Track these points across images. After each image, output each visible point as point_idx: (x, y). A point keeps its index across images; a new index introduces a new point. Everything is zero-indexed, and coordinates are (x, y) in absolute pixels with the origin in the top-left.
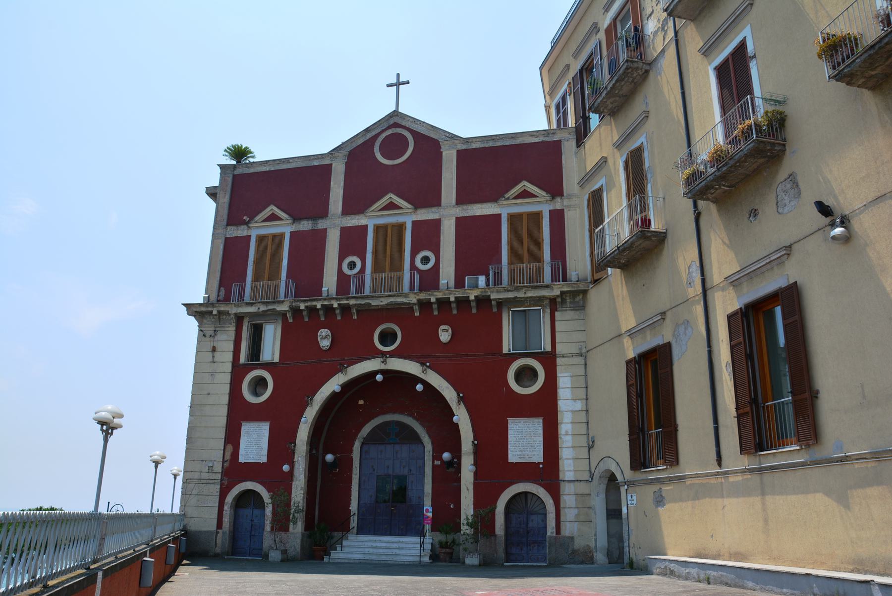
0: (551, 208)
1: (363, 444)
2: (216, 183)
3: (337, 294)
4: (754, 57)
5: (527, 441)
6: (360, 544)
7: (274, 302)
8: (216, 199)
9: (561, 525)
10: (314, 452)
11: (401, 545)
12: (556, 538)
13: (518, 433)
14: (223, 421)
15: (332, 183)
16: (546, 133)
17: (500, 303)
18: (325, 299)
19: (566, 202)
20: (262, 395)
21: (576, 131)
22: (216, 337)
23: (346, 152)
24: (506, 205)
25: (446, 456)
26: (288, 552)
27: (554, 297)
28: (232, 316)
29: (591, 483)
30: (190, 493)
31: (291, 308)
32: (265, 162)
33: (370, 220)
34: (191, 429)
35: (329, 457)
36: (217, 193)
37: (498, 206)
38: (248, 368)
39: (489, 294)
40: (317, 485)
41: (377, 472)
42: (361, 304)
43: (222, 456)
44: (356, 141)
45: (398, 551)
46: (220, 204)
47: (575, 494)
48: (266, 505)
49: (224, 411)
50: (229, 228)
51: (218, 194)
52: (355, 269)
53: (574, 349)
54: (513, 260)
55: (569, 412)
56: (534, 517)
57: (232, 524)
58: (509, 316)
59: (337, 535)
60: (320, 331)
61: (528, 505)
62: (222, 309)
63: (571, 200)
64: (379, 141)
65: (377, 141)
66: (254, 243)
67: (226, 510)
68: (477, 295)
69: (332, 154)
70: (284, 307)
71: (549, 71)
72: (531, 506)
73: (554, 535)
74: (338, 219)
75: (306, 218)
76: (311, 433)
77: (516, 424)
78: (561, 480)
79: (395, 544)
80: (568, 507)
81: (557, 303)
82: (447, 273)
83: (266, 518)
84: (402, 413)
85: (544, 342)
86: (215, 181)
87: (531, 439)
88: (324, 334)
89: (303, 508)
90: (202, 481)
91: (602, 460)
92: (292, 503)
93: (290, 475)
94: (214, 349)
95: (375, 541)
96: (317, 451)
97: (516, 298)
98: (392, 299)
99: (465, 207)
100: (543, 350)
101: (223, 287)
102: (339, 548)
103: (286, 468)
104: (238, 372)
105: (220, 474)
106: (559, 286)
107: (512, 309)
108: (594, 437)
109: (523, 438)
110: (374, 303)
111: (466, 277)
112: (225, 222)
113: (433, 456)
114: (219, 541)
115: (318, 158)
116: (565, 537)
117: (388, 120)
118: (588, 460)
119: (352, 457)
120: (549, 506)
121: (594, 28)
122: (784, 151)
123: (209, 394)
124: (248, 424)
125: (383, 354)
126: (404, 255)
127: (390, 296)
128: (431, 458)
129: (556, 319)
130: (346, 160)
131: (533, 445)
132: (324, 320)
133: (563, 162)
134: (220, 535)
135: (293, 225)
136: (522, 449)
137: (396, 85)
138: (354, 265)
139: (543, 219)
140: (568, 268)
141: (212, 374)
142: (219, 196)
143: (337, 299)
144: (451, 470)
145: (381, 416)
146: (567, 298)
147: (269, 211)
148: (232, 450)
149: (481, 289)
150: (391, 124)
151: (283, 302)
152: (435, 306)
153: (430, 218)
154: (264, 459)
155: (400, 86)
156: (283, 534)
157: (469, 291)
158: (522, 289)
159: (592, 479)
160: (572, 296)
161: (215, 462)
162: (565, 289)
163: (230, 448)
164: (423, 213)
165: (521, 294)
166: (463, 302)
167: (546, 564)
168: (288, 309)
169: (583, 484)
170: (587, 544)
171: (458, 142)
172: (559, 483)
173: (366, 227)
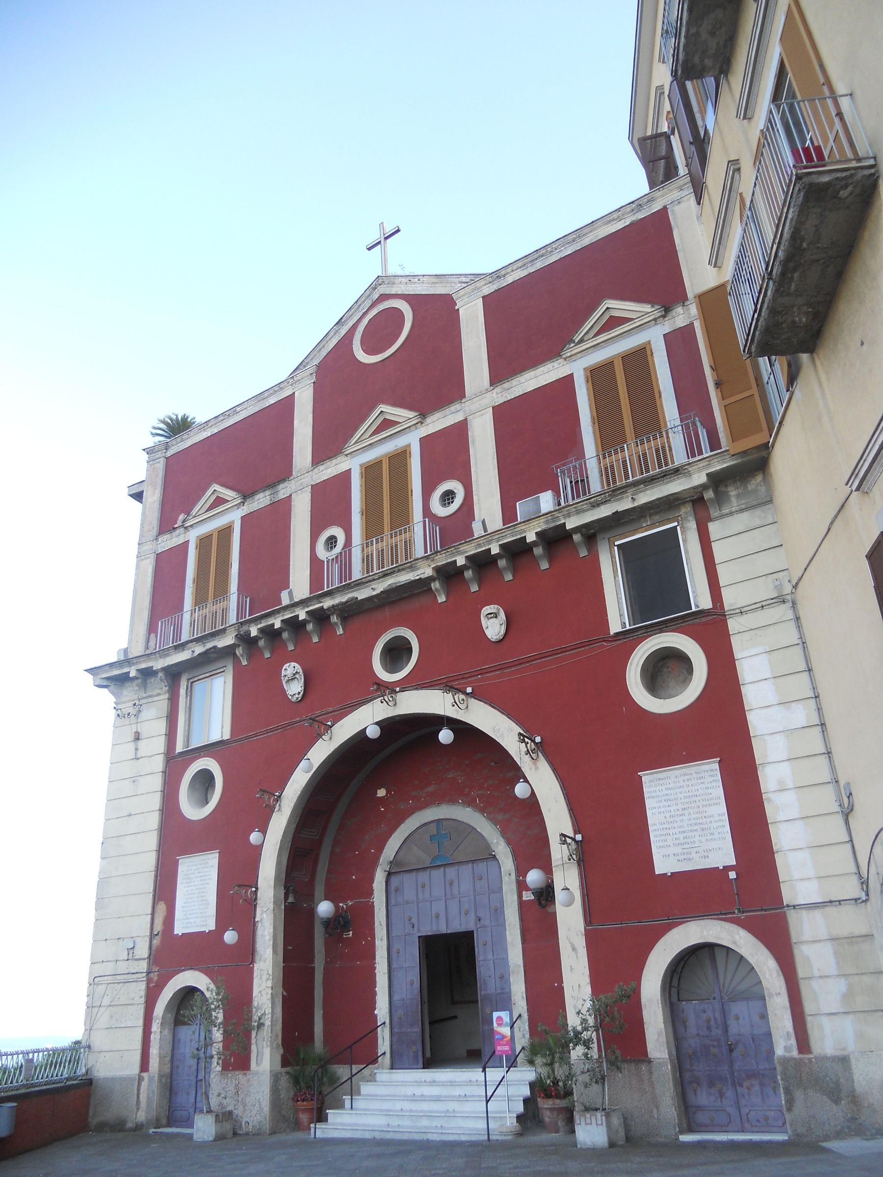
0: (667, 329)
1: (389, 874)
5: (690, 820)
9: (809, 1025)
13: (667, 804)
14: (151, 860)
16: (637, 204)
21: (692, 181)
23: (311, 368)
25: (534, 877)
29: (868, 903)
34: (103, 882)
39: (563, 522)
40: (313, 969)
41: (419, 931)
43: (149, 925)
46: (147, 506)
47: (833, 939)
53: (764, 591)
55: (778, 736)
56: (738, 1008)
59: (342, 1071)
60: (284, 668)
61: (721, 981)
67: (155, 1032)
68: (539, 530)
73: (795, 1053)
76: (285, 862)
77: (661, 782)
78: (788, 906)
84: (453, 801)
90: (118, 977)
91: (877, 837)
99: (506, 385)
100: (694, 609)
106: (701, 464)
107: (616, 543)
108: (848, 784)
109: (680, 812)
111: (517, 504)
112: (155, 532)
116: (823, 1058)
118: (849, 846)
120: (767, 976)
123: (130, 815)
126: (412, 500)
128: (514, 886)
129: (713, 537)
131: (705, 826)
133: (677, 241)
134: (144, 1084)
141: (134, 780)
145: (416, 814)
158: (626, 492)
159: (867, 895)
162: (717, 467)
163: (162, 907)
169: (848, 909)
171: (483, 282)
172: (785, 915)
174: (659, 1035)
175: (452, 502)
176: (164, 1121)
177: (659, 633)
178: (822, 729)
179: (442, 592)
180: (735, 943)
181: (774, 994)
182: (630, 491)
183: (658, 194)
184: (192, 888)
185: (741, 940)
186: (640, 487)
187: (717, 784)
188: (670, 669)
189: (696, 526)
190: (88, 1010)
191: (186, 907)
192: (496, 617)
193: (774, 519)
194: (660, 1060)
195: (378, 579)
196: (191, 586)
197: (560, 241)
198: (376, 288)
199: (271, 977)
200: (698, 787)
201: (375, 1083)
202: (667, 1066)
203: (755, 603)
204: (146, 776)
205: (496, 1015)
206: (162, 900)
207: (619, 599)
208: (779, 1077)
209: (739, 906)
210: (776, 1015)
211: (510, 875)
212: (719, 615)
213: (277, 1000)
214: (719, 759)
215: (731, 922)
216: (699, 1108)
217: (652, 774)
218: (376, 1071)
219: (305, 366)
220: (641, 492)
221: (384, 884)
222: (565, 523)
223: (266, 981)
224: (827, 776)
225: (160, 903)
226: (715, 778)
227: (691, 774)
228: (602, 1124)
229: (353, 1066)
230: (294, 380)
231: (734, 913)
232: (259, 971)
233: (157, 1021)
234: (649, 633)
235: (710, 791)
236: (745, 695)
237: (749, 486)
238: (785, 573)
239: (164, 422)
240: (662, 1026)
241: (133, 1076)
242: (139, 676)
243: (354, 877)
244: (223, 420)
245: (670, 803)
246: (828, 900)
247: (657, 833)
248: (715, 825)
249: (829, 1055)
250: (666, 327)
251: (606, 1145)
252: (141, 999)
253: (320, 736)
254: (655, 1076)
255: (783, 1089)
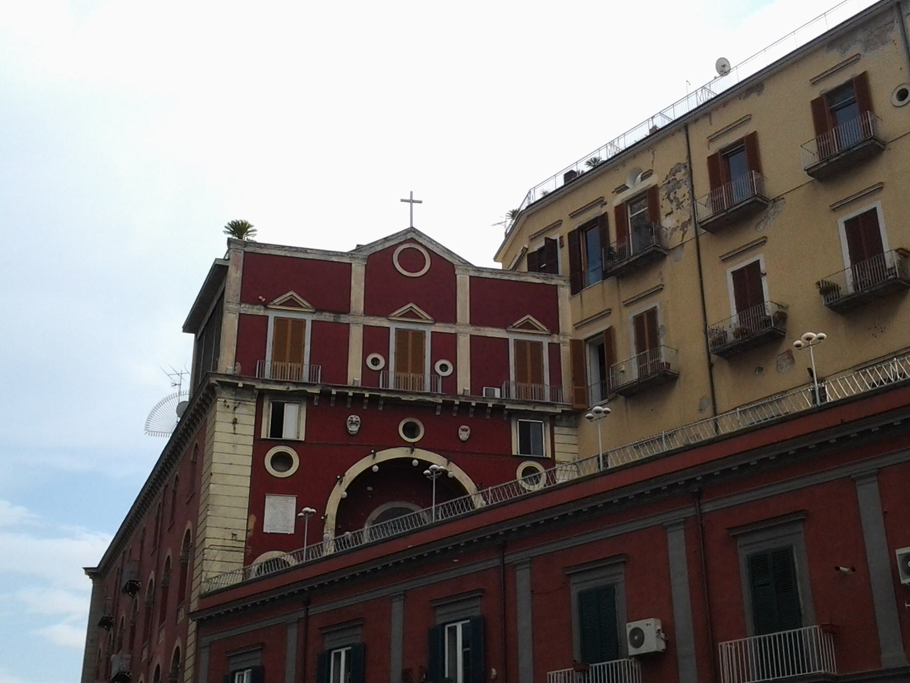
4: (765, 274)
33: (392, 325)
38: (269, 444)
60: (351, 416)
64: (397, 252)
69: (351, 254)
82: (464, 383)
84: (410, 501)
88: (354, 419)
94: (235, 422)
104: (260, 448)
107: (519, 420)
117: (405, 234)
122: (784, 336)
163: (253, 518)
166: (482, 407)
205: (720, 644)
219: (360, 252)
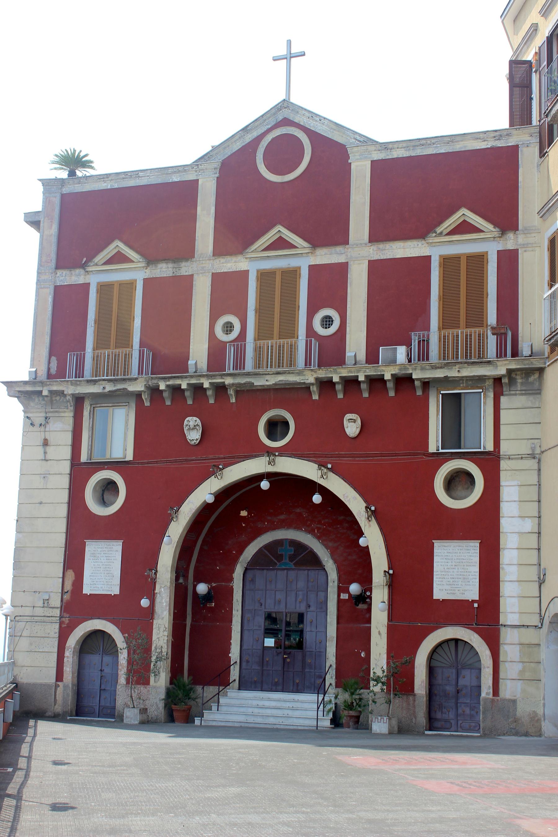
2: (38, 207)
3: (209, 369)
5: (458, 572)
6: (243, 702)
7: (124, 380)
8: (39, 230)
9: (500, 683)
10: (181, 581)
11: (295, 705)
12: (493, 700)
13: (446, 561)
14: (61, 539)
15: (199, 209)
16: (498, 134)
17: (426, 384)
18: (192, 377)
19: (521, 239)
20: (112, 503)
22: (48, 426)
23: (216, 163)
24: (438, 244)
25: (355, 588)
26: (148, 711)
27: (499, 377)
28: (68, 398)
29: (541, 629)
30: (19, 634)
31: (148, 387)
32: (105, 177)
34: (18, 551)
35: (202, 588)
36: (40, 221)
37: (427, 245)
39: (411, 372)
40: (186, 624)
42: (240, 384)
43: (61, 585)
44: (230, 146)
45: (290, 713)
48: (119, 650)
49: (62, 526)
50: (59, 272)
51: (41, 222)
52: (233, 333)
53: (524, 448)
54: (445, 324)
55: (514, 535)
57: (76, 675)
58: (438, 401)
59: (211, 690)
62: (55, 388)
63: (529, 235)
65: (260, 146)
66: (95, 294)
68: (394, 373)
69: (198, 165)
70: (138, 387)
71: (514, 21)
72: (451, 660)
73: (491, 696)
74: (208, 261)
75: (165, 260)
77: (445, 548)
78: (502, 625)
79: (288, 703)
80: (509, 660)
81: (503, 385)
83: (120, 667)
84: (298, 528)
85: (484, 438)
86: (37, 205)
87: (463, 569)
88: (192, 424)
89: (167, 654)
90: (36, 618)
91: (552, 599)
92: (153, 648)
93: (150, 612)
95: (262, 699)
96: (186, 577)
97: (446, 377)
98: (281, 378)
99: (381, 246)
100: (482, 450)
101: (54, 356)
102: (214, 708)
103: (145, 603)
105: (59, 609)
107: (442, 392)
108: (545, 569)
109: (453, 567)
110: (259, 382)
111: (381, 348)
112: (53, 264)
113: (339, 587)
114: (59, 697)
115: (179, 171)
116: (504, 700)
117: (274, 114)
118: (538, 599)
119: (232, 587)
120: (484, 658)
121: (533, 31)
123: (41, 503)
124: (94, 543)
125: (270, 452)
127: (278, 373)
128: (336, 590)
130: (217, 175)
131: (466, 577)
132: (191, 403)
134: (60, 690)
135: (146, 269)
136: (451, 583)
137: (286, 58)
138: (231, 327)
139: (489, 264)
140: (520, 335)
141: (45, 476)
142: (44, 227)
143: (208, 376)
144: (361, 606)
146: (518, 377)
147: (113, 249)
148: (74, 578)
149: (399, 365)
150: (279, 120)
151: (136, 379)
152: (339, 387)
153: (333, 262)
154: (115, 590)
155: (292, 59)
156: (142, 688)
157: (383, 368)
159: (542, 625)
160: (524, 375)
161: (51, 594)
162: (513, 366)
163: (71, 575)
164: (323, 254)
165: (453, 373)
167: (479, 735)
168: (143, 389)
169: (531, 630)
170: (533, 710)
171: (373, 148)
172: (498, 631)
173: (245, 273)
174: (422, 682)
175: (329, 327)
176: (74, 713)
177: (459, 459)
178: (539, 535)
179: (317, 393)
180: (471, 640)
181: (486, 667)
182: (457, 366)
183: (514, 132)
184: (99, 564)
185: (474, 639)
186: (465, 365)
187: (477, 555)
188: (460, 480)
189: (493, 396)
190: (11, 638)
191: (93, 576)
192: (355, 422)
193: (539, 405)
194: (420, 695)
195: (272, 374)
196: (93, 325)
197: (438, 138)
198: (281, 110)
199: (167, 630)
200: (466, 555)
201: (226, 697)
202: (424, 698)
203: (518, 455)
204: (54, 475)
206: (70, 569)
207: (437, 430)
208: (481, 707)
209: (476, 621)
210: (485, 677)
211: (334, 582)
212: (496, 456)
213: (169, 644)
214: (480, 541)
215: (471, 630)
216: (436, 719)
217: (441, 542)
218: (227, 691)
220: (465, 368)
221: (242, 576)
222: (412, 373)
223: (163, 632)
224: (535, 561)
225: (69, 570)
226: (475, 551)
227: (463, 547)
228: (386, 723)
229: (220, 687)
230: (198, 168)
231: (473, 625)
232: (157, 625)
233: (70, 650)
234: (453, 457)
235: (472, 558)
236: (502, 508)
237: (530, 379)
238: (539, 441)
239: (56, 156)
240: (425, 678)
241: (51, 684)
242: (49, 395)
243: (218, 568)
244: (124, 178)
245: (448, 561)
246: (522, 625)
247: (438, 576)
248: (471, 577)
249: (507, 698)
250: (500, 246)
251: (387, 732)
252: (56, 635)
253: (213, 473)
254: (417, 702)
255: (482, 712)
